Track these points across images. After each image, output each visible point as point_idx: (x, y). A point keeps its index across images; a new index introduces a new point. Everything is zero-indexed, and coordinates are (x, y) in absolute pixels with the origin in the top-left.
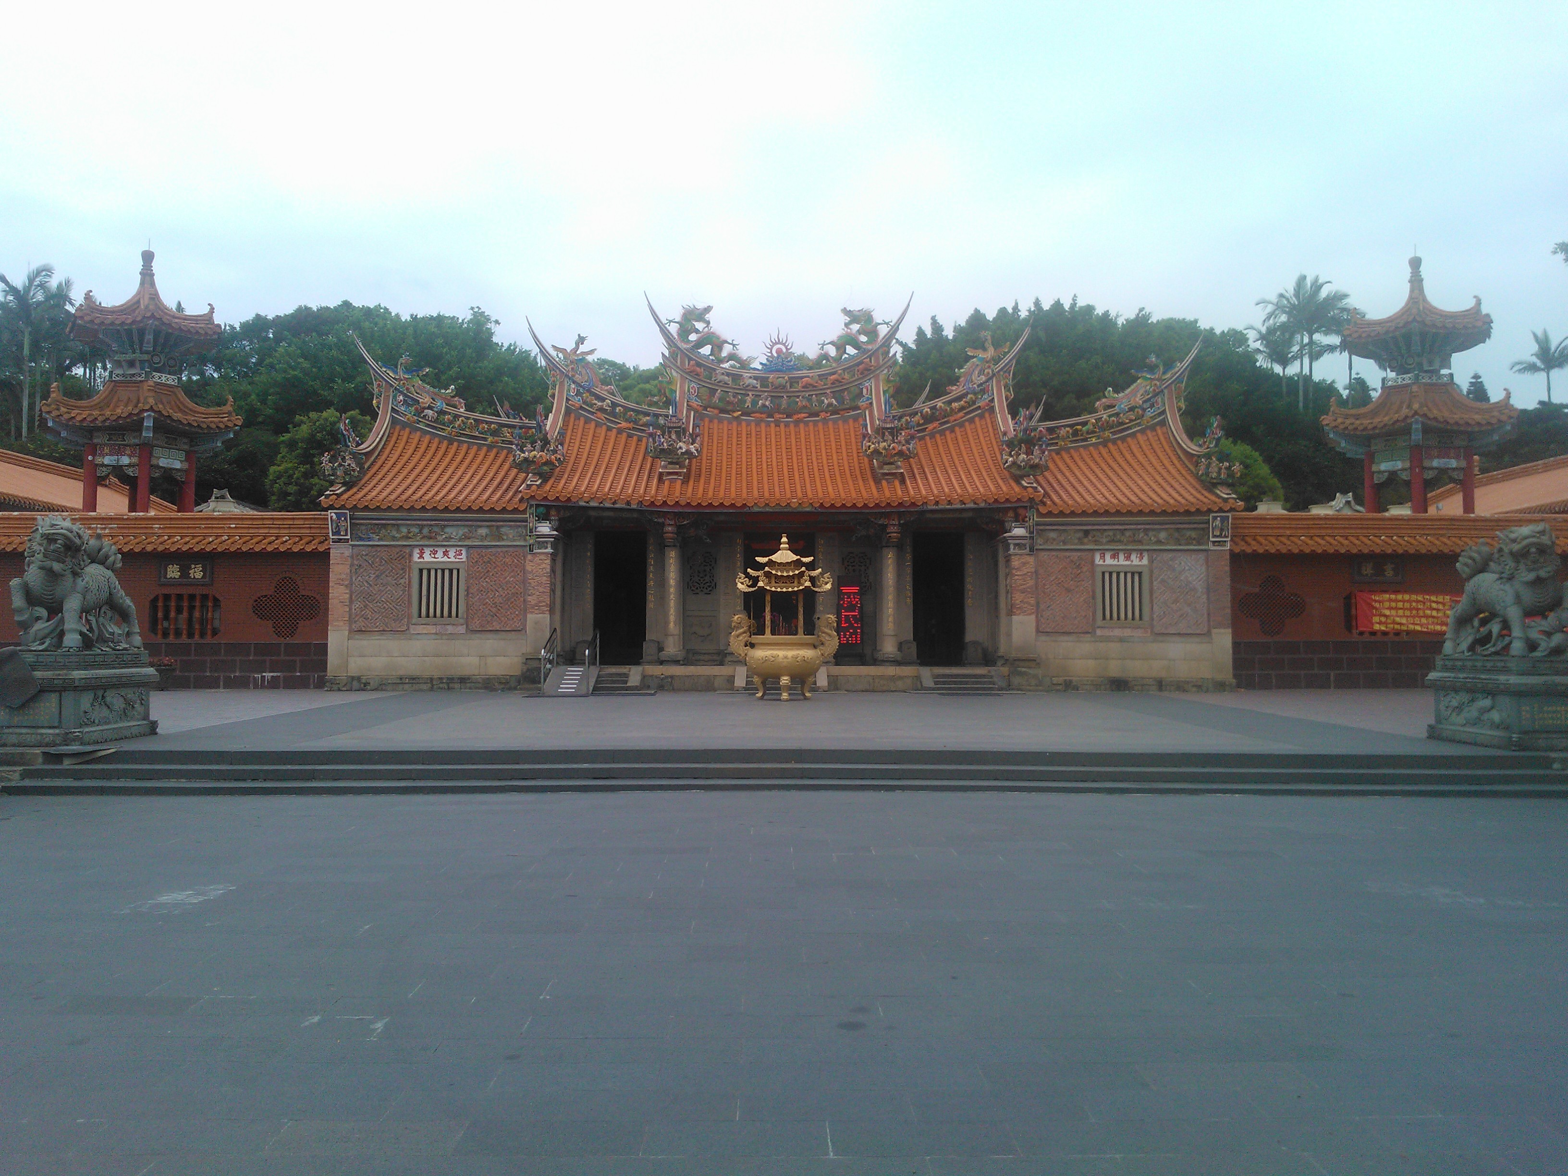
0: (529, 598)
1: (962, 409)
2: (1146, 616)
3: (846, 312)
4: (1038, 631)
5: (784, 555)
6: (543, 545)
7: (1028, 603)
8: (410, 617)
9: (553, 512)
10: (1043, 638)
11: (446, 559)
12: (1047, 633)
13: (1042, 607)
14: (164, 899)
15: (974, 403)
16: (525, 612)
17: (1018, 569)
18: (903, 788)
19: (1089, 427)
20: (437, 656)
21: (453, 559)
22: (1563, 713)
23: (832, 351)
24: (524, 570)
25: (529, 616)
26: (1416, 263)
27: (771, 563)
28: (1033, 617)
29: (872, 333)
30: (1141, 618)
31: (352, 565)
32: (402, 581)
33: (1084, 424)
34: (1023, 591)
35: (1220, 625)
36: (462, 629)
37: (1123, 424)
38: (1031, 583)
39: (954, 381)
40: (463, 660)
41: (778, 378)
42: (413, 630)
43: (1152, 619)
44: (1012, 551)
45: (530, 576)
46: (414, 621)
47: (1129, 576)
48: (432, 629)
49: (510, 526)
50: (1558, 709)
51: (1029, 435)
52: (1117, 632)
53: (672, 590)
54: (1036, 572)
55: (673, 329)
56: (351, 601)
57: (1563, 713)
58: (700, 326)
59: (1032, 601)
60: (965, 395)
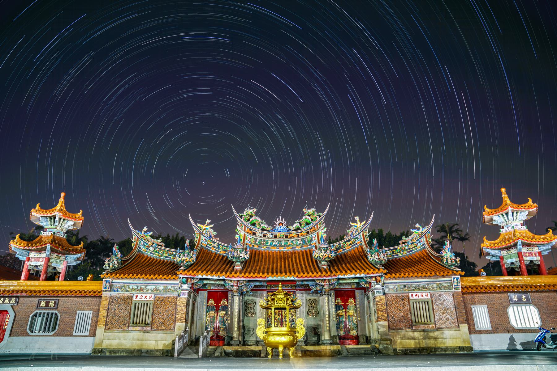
0: (177, 316)
1: (350, 244)
2: (433, 321)
8: (129, 323)
9: (189, 280)
10: (391, 331)
11: (146, 299)
12: (393, 329)
14: (372, 216)
16: (175, 321)
19: (398, 250)
20: (138, 340)
21: (148, 299)
24: (176, 304)
25: (177, 323)
31: (109, 301)
32: (128, 308)
33: (396, 249)
34: (382, 311)
35: (462, 323)
36: (149, 329)
37: (410, 249)
38: (384, 307)
39: (347, 234)
40: (148, 342)
41: (266, 277)
42: (131, 328)
43: (435, 321)
44: (376, 295)
45: (178, 307)
46: (131, 325)
47: (423, 303)
49: (524, 289)
51: (444, 233)
56: (107, 316)
59: (386, 315)
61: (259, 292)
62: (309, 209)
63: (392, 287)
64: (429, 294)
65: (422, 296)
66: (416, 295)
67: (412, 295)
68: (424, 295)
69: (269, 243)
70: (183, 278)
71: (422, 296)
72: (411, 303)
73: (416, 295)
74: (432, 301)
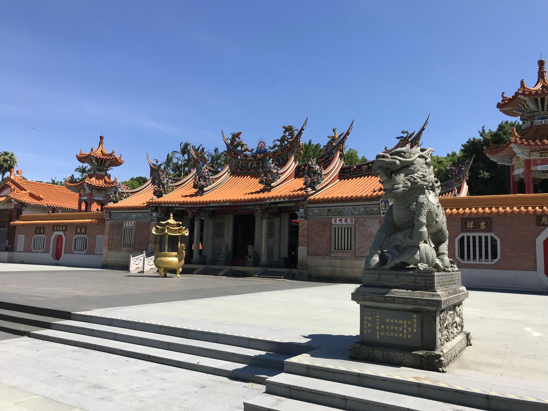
1: (323, 161)
2: (353, 248)
3: (284, 127)
4: (308, 254)
5: (171, 221)
6: (154, 220)
7: (304, 241)
10: (310, 257)
12: (312, 255)
13: (310, 243)
15: (328, 158)
17: (301, 227)
18: (29, 335)
22: (405, 326)
23: (278, 143)
26: (541, 63)
27: (168, 223)
28: (306, 247)
29: (291, 134)
30: (351, 249)
34: (303, 236)
38: (306, 232)
43: (355, 248)
48: (126, 249)
50: (401, 322)
52: (340, 255)
53: (195, 236)
54: (308, 227)
55: (229, 142)
57: (405, 326)
58: (237, 139)
59: (306, 240)
60: (324, 156)
61: (227, 215)
62: (486, 172)
63: (316, 211)
64: (353, 219)
65: (346, 221)
66: (340, 220)
67: (335, 221)
68: (348, 221)
69: (249, 166)
70: (152, 207)
71: (346, 221)
72: (333, 230)
73: (340, 220)
74: (355, 228)
